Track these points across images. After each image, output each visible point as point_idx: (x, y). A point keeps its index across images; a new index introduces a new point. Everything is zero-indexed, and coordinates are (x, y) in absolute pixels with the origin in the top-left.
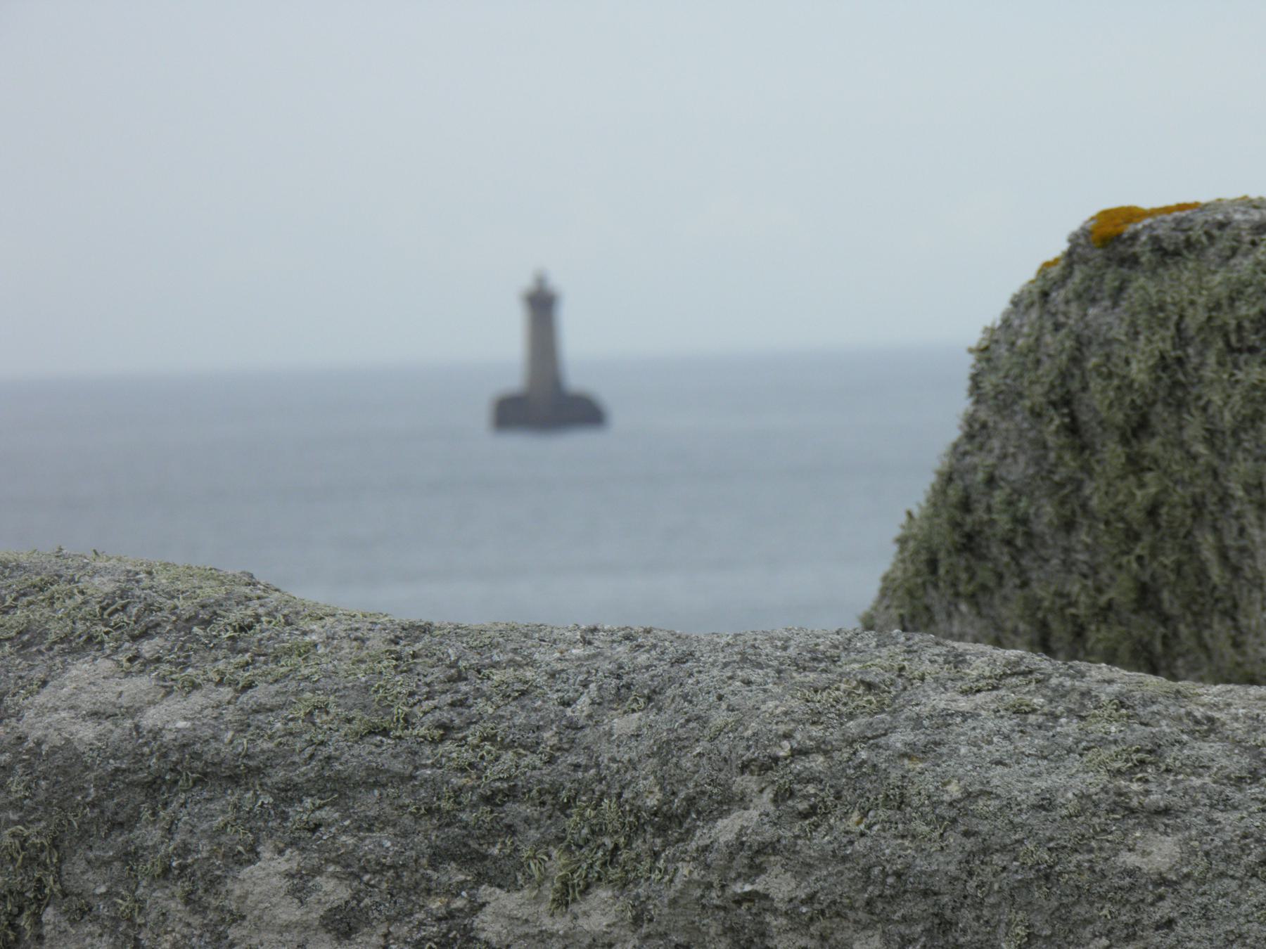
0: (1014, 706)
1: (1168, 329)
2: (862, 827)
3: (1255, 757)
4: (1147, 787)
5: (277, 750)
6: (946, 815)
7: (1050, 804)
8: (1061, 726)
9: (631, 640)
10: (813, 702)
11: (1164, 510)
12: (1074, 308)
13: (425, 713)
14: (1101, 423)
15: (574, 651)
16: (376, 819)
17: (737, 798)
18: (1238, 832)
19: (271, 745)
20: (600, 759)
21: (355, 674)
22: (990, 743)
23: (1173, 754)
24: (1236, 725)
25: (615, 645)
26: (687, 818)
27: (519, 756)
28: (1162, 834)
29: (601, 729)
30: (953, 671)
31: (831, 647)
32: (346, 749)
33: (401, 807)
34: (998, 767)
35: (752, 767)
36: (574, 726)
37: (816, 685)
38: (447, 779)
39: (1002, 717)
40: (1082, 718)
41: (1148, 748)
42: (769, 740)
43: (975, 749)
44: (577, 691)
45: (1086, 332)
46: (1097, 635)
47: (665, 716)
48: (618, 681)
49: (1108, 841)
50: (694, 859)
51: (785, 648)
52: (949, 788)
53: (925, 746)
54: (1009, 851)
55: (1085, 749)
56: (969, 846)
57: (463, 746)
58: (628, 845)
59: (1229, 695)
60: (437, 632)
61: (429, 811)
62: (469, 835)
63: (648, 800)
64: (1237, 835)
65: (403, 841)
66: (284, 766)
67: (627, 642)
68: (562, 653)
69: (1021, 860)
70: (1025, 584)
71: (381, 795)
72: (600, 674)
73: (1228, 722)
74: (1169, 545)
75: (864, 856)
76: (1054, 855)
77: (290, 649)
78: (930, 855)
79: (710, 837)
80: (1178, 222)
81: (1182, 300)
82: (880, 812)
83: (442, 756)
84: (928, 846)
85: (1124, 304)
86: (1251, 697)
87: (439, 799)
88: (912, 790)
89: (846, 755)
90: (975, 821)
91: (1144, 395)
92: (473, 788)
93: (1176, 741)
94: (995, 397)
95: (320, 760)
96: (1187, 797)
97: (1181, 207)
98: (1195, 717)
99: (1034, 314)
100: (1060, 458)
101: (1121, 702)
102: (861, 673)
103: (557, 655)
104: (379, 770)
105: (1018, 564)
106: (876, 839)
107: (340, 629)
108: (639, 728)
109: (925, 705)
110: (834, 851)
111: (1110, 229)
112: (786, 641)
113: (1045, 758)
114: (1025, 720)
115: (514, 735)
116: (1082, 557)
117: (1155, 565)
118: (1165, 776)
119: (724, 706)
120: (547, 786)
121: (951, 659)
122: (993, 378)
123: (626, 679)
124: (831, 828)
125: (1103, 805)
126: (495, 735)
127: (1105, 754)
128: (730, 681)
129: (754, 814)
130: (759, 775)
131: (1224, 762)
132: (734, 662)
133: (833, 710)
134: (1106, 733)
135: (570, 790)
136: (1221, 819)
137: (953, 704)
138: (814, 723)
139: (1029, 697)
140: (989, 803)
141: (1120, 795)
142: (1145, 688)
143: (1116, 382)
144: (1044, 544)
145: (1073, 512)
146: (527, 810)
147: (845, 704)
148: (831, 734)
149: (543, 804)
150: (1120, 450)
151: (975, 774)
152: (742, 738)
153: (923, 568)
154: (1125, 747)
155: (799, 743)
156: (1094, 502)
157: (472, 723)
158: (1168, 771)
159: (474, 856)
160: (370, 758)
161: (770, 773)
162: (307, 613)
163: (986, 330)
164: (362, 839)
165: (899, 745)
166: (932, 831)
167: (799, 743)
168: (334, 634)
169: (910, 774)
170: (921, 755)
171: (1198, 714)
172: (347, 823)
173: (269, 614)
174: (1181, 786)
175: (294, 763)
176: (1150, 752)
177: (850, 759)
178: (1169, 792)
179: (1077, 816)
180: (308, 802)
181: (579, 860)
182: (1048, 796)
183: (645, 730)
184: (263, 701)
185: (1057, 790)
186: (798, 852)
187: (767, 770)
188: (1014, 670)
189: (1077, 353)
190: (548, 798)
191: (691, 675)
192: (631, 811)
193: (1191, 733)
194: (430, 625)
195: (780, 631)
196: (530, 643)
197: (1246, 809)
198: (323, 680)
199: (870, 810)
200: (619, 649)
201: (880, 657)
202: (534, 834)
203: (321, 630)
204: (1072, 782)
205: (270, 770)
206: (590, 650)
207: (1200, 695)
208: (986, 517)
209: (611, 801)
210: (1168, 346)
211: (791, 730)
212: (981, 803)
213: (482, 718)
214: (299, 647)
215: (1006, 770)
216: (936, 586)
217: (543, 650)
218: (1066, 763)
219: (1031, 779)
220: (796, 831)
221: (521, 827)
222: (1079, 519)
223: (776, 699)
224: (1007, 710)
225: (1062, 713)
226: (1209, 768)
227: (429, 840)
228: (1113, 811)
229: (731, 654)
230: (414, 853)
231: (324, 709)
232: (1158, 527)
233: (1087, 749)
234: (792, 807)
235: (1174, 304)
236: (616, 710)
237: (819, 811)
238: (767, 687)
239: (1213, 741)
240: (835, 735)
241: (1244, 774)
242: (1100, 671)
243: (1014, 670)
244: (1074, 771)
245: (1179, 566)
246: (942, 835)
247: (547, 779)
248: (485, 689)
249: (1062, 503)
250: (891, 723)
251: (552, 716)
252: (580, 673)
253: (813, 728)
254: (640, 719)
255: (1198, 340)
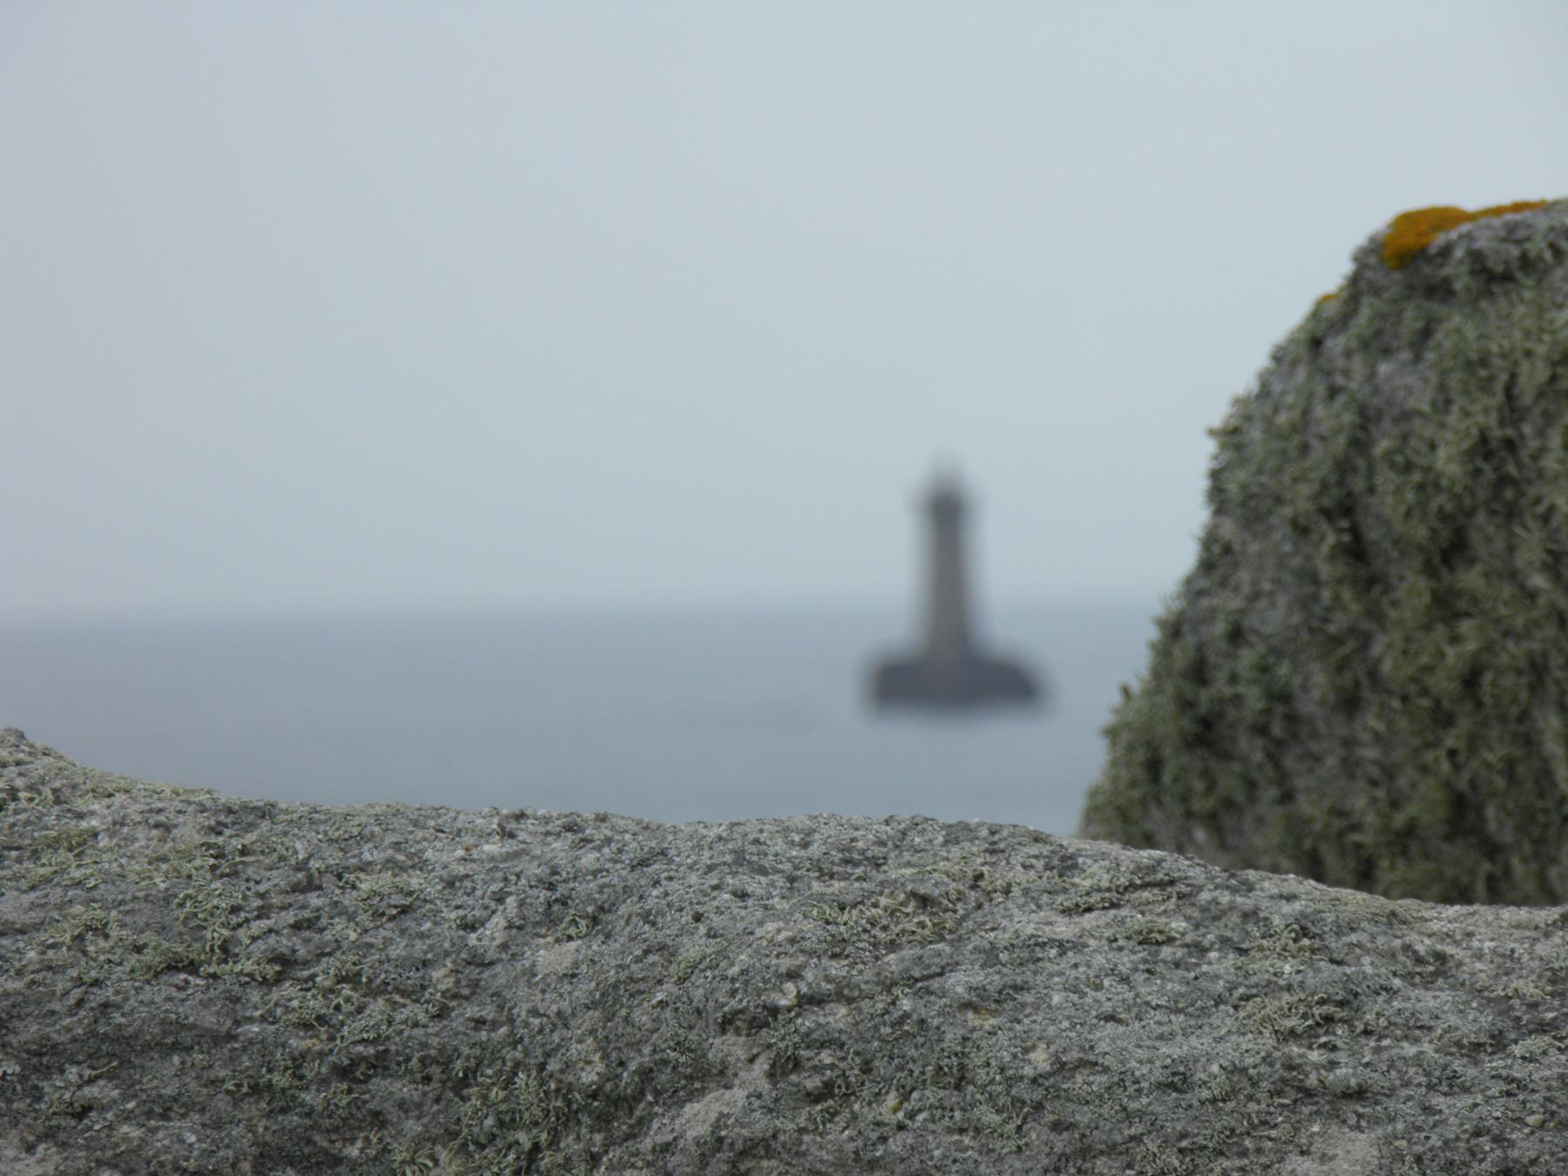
0: (1140, 933)
1: (1494, 394)
2: (900, 1115)
3: (1501, 1013)
4: (1332, 1056)
5: (28, 992)
6: (1026, 1097)
7: (1185, 1080)
8: (1210, 963)
9: (575, 832)
10: (837, 924)
11: (1488, 677)
12: (1358, 365)
13: (254, 939)
14: (1396, 542)
15: (486, 848)
16: (175, 1100)
17: (715, 1071)
18: (1466, 1127)
19: (19, 985)
20: (515, 1011)
21: (151, 878)
22: (1098, 987)
23: (1376, 1008)
24: (1478, 965)
25: (550, 839)
26: (640, 1101)
27: (395, 1006)
28: (1352, 1128)
29: (519, 966)
30: (1057, 879)
31: (874, 843)
32: (133, 992)
33: (213, 1082)
34: (1108, 1025)
35: (739, 1023)
36: (479, 961)
37: (842, 899)
38: (283, 1039)
39: (1120, 949)
40: (1243, 952)
41: (1339, 998)
42: (765, 982)
43: (1075, 997)
44: (486, 908)
45: (1376, 401)
46: (1386, 871)
47: (615, 946)
48: (549, 893)
49: (1270, 1139)
50: (649, 1164)
51: (805, 845)
52: (1032, 1056)
53: (1000, 992)
54: (1121, 1153)
55: (1241, 999)
56: (1060, 1144)
57: (308, 990)
58: (554, 1143)
59: (1471, 920)
60: (282, 817)
61: (255, 1089)
62: (315, 1127)
63: (584, 1074)
64: (1465, 1131)
65: (215, 1134)
66: (37, 1017)
67: (569, 835)
68: (467, 850)
69: (1137, 1168)
70: (1287, 797)
71: (183, 1063)
72: (523, 881)
73: (1467, 960)
74: (1495, 732)
75: (903, 1160)
76: (1187, 1159)
77: (57, 840)
78: (1000, 1159)
79: (673, 1130)
80: (1511, 228)
81: (1513, 350)
82: (928, 1093)
83: (277, 1005)
84: (998, 1145)
85: (1430, 356)
86: (1504, 924)
87: (270, 1071)
88: (977, 1059)
89: (880, 1005)
90: (1071, 1106)
91: (1456, 497)
92: (322, 1055)
93: (1382, 988)
94: (1243, 504)
95: (92, 1009)
96: (1394, 1073)
97: (1518, 207)
98: (1415, 952)
99: (1301, 375)
100: (1337, 598)
101: (1303, 928)
102: (913, 881)
103: (460, 853)
104: (181, 1026)
105: (1277, 764)
106: (920, 1134)
107: (134, 810)
108: (576, 965)
109: (1004, 929)
110: (856, 1153)
111: (1410, 241)
112: (808, 835)
113: (1178, 1011)
114: (1157, 953)
115: (389, 973)
116: (1370, 753)
117: (1474, 764)
118: (1363, 1040)
119: (702, 930)
120: (433, 1052)
121: (1055, 862)
122: (1242, 475)
123: (562, 890)
124: (855, 1117)
125: (1264, 1084)
126: (359, 974)
127: (1272, 1006)
128: (715, 893)
129: (738, 1095)
130: (748, 1035)
131: (1454, 1020)
132: (725, 864)
133: (865, 936)
134: (1275, 974)
135: (468, 1058)
136: (1443, 1107)
137: (1047, 929)
138: (834, 956)
139: (1164, 920)
140: (1091, 1079)
141: (1291, 1068)
142: (1342, 908)
143: (1416, 477)
144: (1315, 734)
145: (1357, 684)
146: (403, 1089)
147: (885, 928)
148: (860, 972)
149: (427, 1079)
150: (1423, 583)
151: (1073, 1034)
152: (724, 978)
153: (1140, 773)
154: (1303, 996)
155: (809, 985)
156: (1387, 666)
157: (324, 955)
158: (1367, 1033)
159: (322, 1158)
160: (168, 1006)
161: (764, 1032)
162: (89, 786)
163: (1238, 401)
164: (153, 1131)
165: (960, 990)
166: (1006, 1121)
167: (809, 985)
168: (124, 817)
169: (975, 1035)
170: (993, 1006)
171: (1421, 949)
172: (131, 1105)
173: (31, 788)
174: (1385, 1056)
175: (53, 1013)
176: (1341, 1004)
177: (887, 1012)
178: (1367, 1065)
179: (1224, 1101)
180: (72, 1073)
181: (480, 1167)
182: (1182, 1069)
183: (584, 968)
184: (10, 917)
185: (1196, 1061)
186: (804, 1154)
187: (761, 1027)
188: (1147, 880)
189: (1360, 434)
190: (435, 1071)
191: (657, 883)
192: (558, 1090)
193: (1408, 977)
194: (272, 805)
195: (800, 820)
196: (420, 834)
197: (1483, 1091)
198: (102, 886)
199: (913, 1089)
200: (555, 845)
201: (948, 859)
202: (412, 1126)
203: (106, 812)
204: (1220, 1047)
205: (16, 1023)
206: (511, 846)
207: (1427, 921)
208: (1228, 691)
209: (529, 1076)
210: (1493, 419)
211: (799, 966)
212: (1079, 1079)
213: (339, 947)
214: (69, 837)
215: (1121, 1029)
216: (1159, 803)
217: (438, 845)
218: (1213, 1020)
219: (1158, 1044)
220: (802, 1121)
221: (393, 1115)
222: (1367, 693)
223: (779, 919)
224: (1128, 938)
225: (1212, 944)
226: (1430, 1029)
227: (255, 1133)
228: (1280, 1093)
229: (723, 853)
230: (230, 1153)
231: (101, 931)
232: (1479, 704)
233: (1246, 998)
234: (797, 1085)
235: (1503, 356)
236: (544, 936)
237: (836, 1091)
238: (770, 902)
239: (1441, 989)
240: (864, 975)
241: (1483, 1039)
242: (1270, 884)
243: (1147, 879)
244: (1223, 1031)
245: (1510, 766)
246: (1019, 1128)
247: (434, 1041)
248: (347, 902)
249: (1341, 668)
250: (951, 957)
251: (446, 945)
252: (494, 880)
253: (834, 963)
254: (577, 951)
255: (1537, 411)
